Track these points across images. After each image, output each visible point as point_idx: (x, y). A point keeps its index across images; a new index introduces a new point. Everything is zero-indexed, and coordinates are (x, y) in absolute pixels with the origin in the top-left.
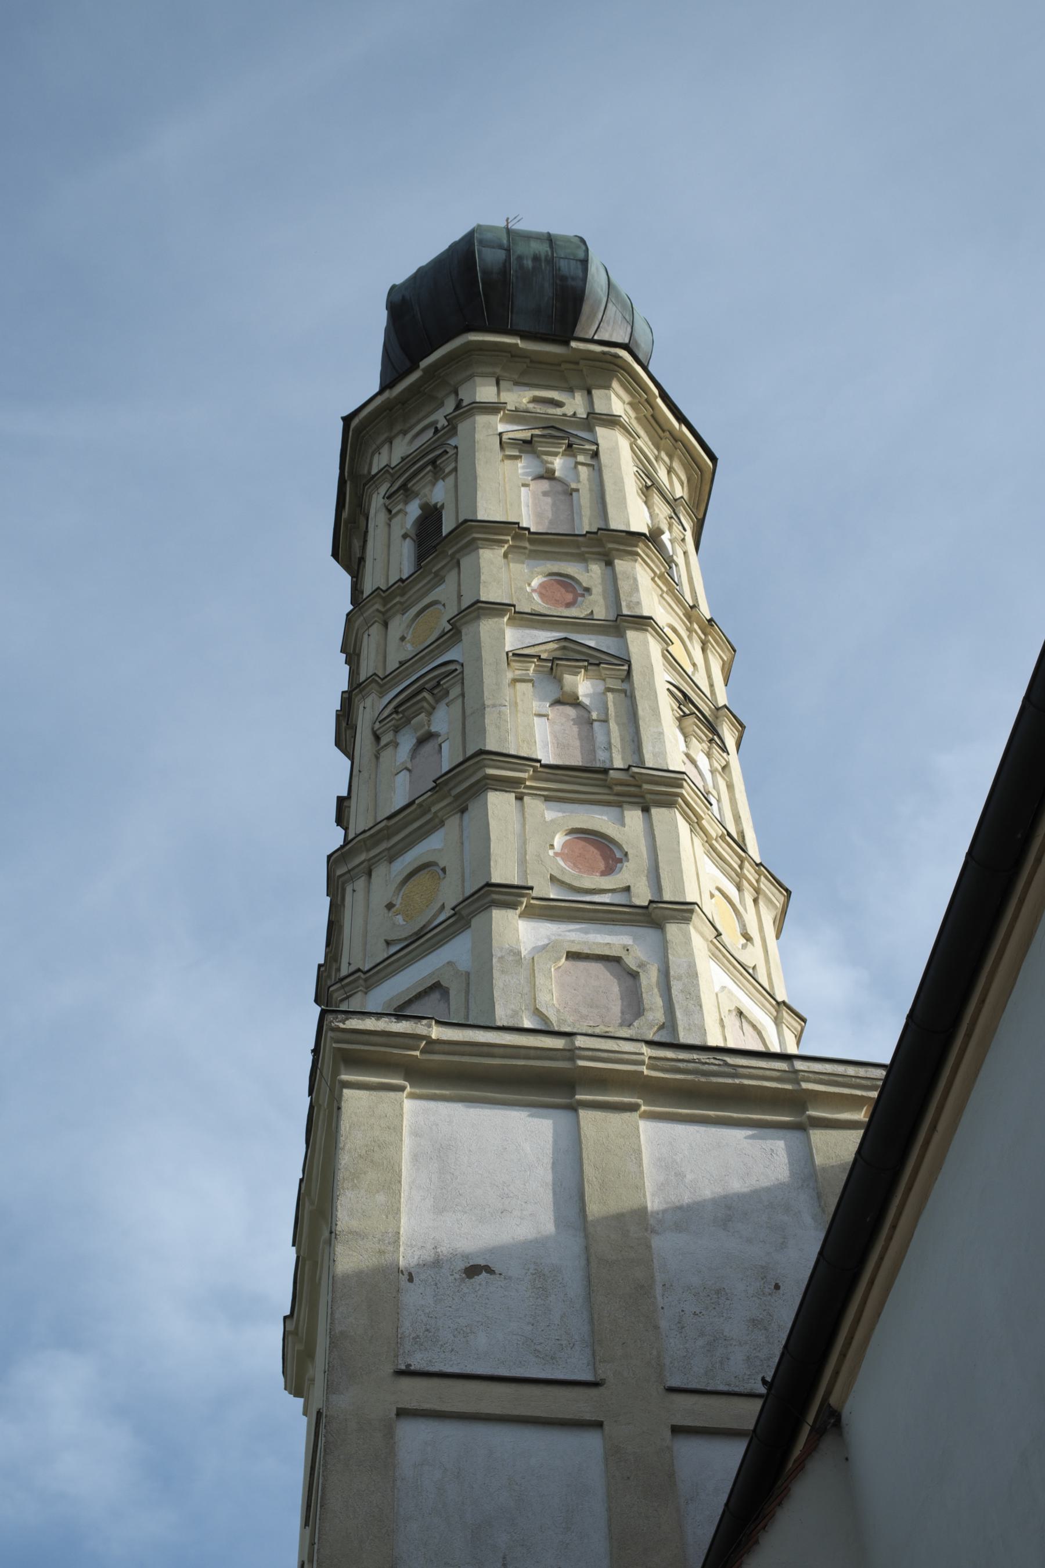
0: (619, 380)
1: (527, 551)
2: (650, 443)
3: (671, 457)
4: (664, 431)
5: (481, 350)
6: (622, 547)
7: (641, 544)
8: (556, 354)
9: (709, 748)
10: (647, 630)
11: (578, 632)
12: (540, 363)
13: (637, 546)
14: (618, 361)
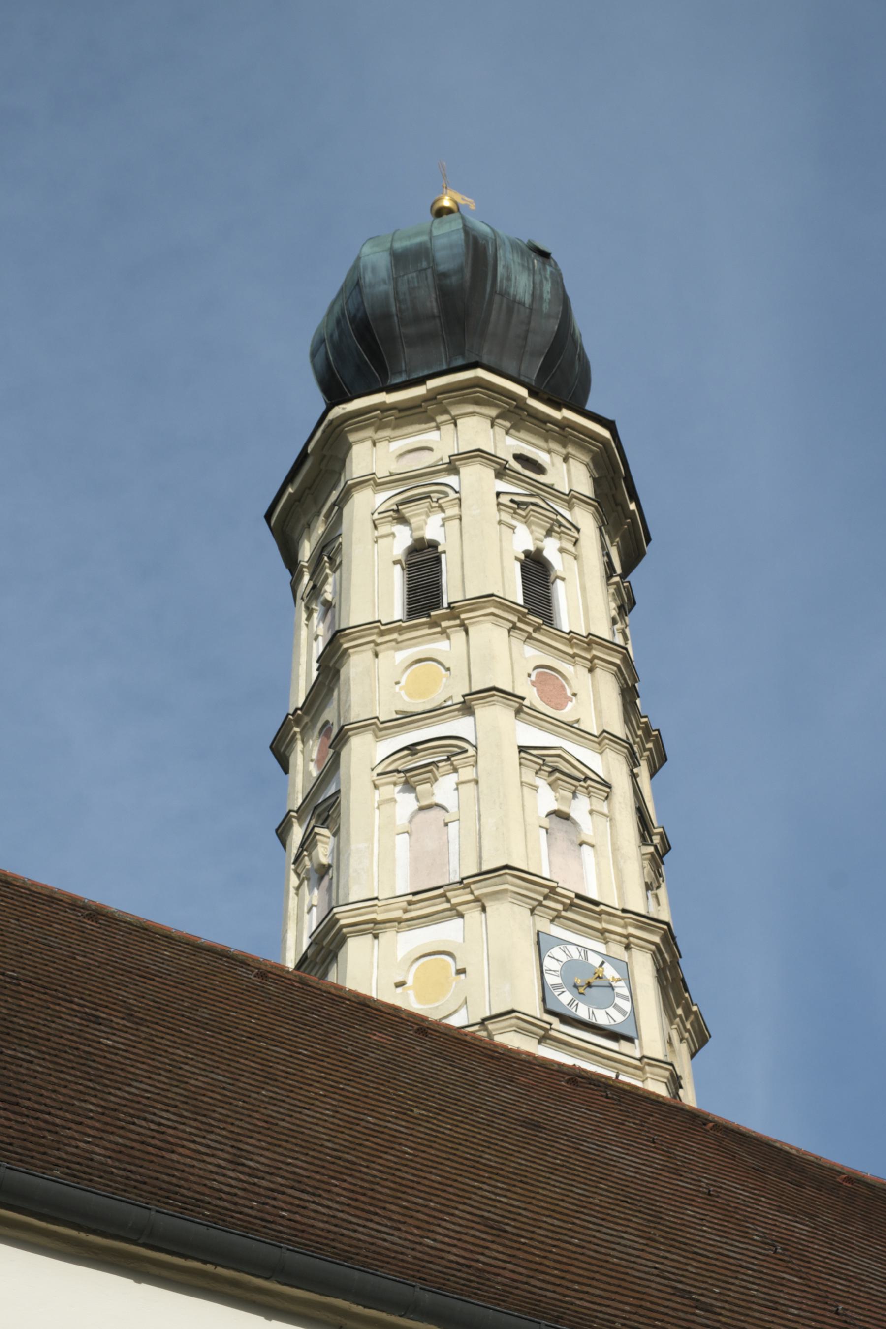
0: (351, 431)
1: (309, 724)
2: (424, 426)
3: (446, 412)
4: (420, 406)
5: (284, 521)
6: (336, 657)
7: (342, 641)
8: (311, 468)
9: (452, 764)
10: (349, 737)
11: (324, 790)
12: (314, 481)
13: (341, 645)
14: (335, 423)
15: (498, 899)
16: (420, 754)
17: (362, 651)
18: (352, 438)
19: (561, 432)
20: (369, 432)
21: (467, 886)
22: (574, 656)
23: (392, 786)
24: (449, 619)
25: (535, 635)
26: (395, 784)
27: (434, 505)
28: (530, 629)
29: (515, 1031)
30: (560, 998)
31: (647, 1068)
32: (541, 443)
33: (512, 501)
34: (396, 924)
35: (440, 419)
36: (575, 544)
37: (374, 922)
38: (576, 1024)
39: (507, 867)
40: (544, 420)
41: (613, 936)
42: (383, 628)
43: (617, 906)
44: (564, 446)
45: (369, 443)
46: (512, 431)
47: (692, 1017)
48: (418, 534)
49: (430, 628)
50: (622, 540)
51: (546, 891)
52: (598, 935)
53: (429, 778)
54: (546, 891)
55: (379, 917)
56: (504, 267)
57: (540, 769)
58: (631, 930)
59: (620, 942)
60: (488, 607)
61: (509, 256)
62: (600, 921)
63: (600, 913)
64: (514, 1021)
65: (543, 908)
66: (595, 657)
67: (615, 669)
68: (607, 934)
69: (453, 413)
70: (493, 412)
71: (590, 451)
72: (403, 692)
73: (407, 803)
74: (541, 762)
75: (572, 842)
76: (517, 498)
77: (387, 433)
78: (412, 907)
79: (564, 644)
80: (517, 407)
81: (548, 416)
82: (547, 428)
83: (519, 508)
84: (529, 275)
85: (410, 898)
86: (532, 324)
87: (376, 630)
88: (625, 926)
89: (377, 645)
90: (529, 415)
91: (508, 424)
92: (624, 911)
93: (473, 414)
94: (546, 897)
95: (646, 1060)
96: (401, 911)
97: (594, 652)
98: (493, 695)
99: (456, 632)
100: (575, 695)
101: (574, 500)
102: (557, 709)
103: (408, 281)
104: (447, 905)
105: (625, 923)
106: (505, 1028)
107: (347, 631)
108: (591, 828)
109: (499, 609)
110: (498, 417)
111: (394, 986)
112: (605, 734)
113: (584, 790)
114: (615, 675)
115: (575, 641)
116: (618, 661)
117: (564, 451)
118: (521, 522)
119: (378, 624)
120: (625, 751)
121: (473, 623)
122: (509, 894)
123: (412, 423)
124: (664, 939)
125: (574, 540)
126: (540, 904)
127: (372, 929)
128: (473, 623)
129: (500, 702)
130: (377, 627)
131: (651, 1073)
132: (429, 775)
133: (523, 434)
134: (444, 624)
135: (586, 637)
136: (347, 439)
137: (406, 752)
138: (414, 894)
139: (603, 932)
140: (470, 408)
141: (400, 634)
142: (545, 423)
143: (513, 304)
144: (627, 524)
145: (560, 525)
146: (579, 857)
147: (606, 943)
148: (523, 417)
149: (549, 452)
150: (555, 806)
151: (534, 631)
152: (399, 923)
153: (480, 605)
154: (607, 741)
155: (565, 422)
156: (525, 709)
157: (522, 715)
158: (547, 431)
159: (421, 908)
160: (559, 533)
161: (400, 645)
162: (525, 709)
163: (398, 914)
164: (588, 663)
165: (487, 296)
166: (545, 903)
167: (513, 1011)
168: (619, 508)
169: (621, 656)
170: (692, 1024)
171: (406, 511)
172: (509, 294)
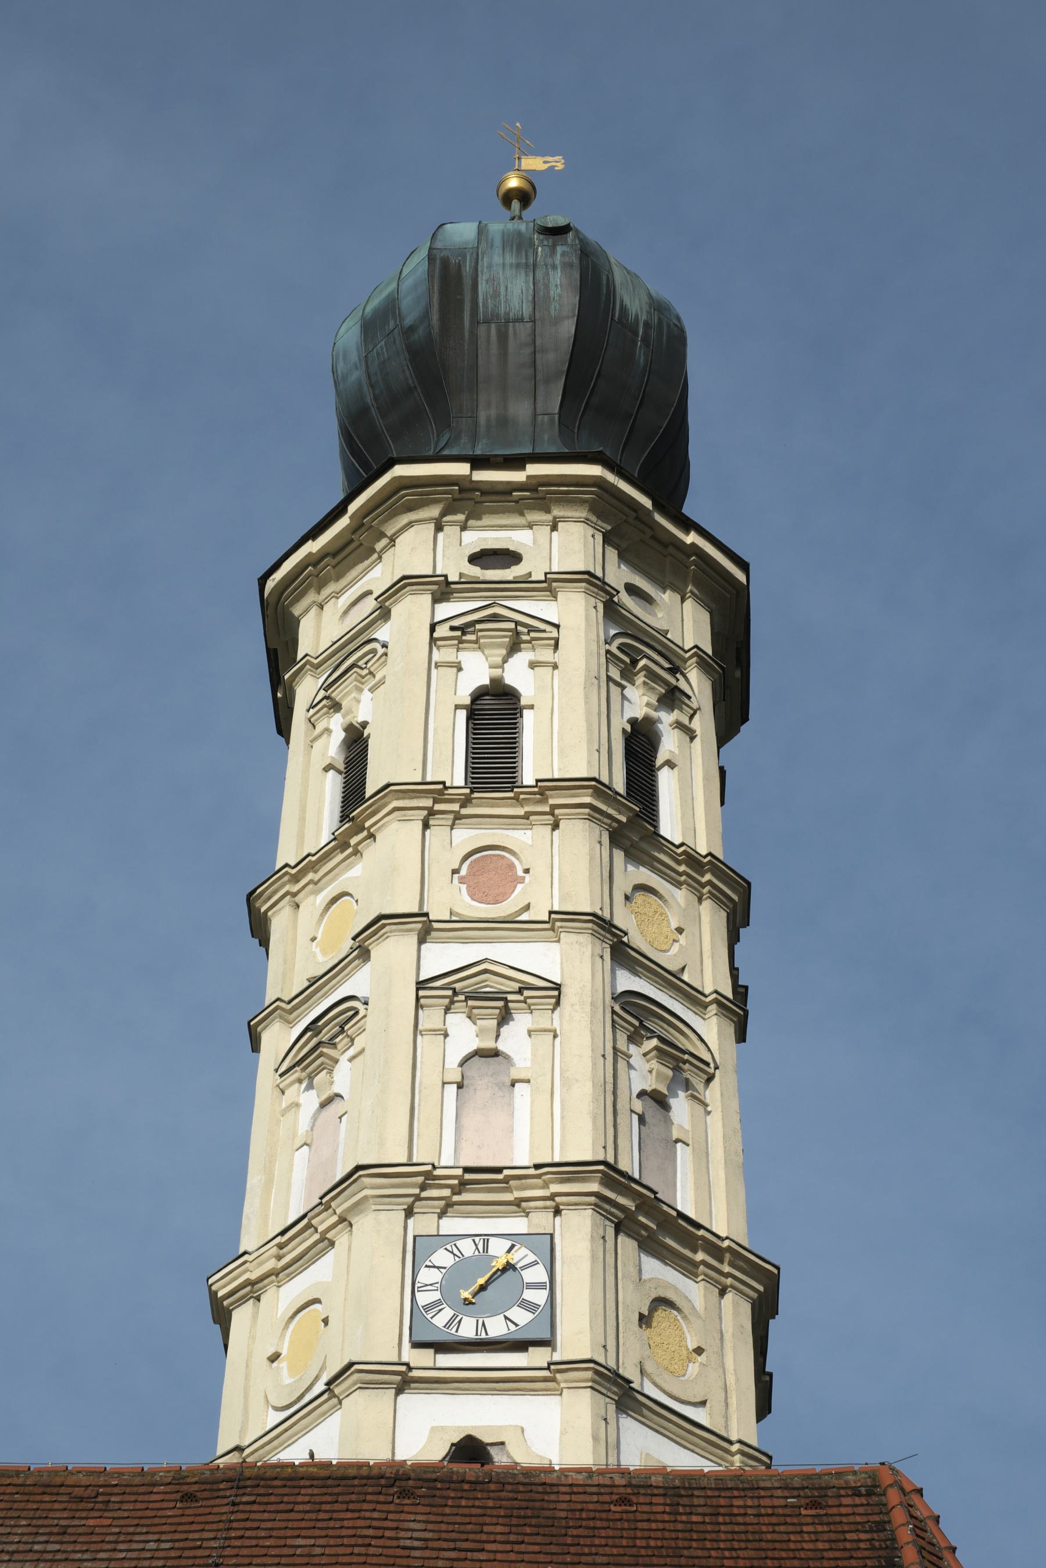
2: (367, 563)
4: (352, 541)
9: (348, 1036)
15: (362, 1212)
16: (324, 1031)
17: (280, 910)
18: (297, 610)
19: (535, 495)
20: (311, 597)
21: (328, 1207)
22: (527, 816)
23: (297, 1085)
24: (357, 834)
25: (464, 811)
26: (300, 1081)
27: (365, 672)
28: (455, 807)
29: (360, 1388)
30: (434, 1321)
31: (558, 1376)
32: (517, 520)
33: (452, 628)
34: (273, 1277)
35: (379, 546)
36: (556, 646)
37: (249, 1283)
38: (463, 1347)
39: (359, 1168)
40: (505, 491)
41: (532, 1204)
42: (294, 871)
43: (527, 1164)
44: (548, 511)
45: (314, 610)
46: (471, 523)
47: (727, 1256)
48: (349, 719)
49: (342, 852)
50: (696, 585)
51: (420, 1179)
52: (514, 1208)
53: (322, 1064)
54: (420, 1179)
55: (253, 1276)
56: (487, 281)
57: (452, 1002)
58: (555, 1188)
59: (545, 1208)
60: (390, 802)
61: (497, 259)
62: (509, 1190)
63: (507, 1180)
64: (356, 1376)
65: (424, 1202)
66: (554, 807)
67: (587, 811)
68: (524, 1204)
69: (389, 532)
70: (435, 511)
71: (583, 501)
72: (318, 951)
73: (310, 1100)
74: (449, 993)
75: (500, 1086)
76: (456, 623)
77: (331, 588)
78: (285, 1250)
79: (511, 806)
80: (461, 491)
81: (508, 483)
82: (514, 499)
83: (464, 633)
84: (527, 275)
85: (278, 1240)
86: (538, 342)
87: (286, 878)
88: (546, 1186)
89: (294, 895)
90: (484, 493)
91: (461, 517)
92: (537, 1167)
93: (410, 525)
94: (423, 1187)
95: (552, 1367)
96: (273, 1260)
97: (551, 801)
98: (384, 926)
99: (368, 846)
100: (527, 871)
101: (554, 584)
102: (496, 902)
103: (378, 354)
104: (316, 1237)
105: (544, 1181)
106: (349, 1388)
107: (258, 891)
108: (529, 1055)
109: (403, 798)
110: (443, 514)
111: (268, 1363)
112: (553, 916)
113: (523, 1005)
114: (590, 819)
115: (522, 796)
116: (587, 800)
117: (549, 517)
118: (474, 649)
119: (287, 869)
120: (590, 925)
121: (379, 828)
122: (371, 1201)
123: (355, 565)
124: (607, 1181)
125: (553, 642)
126: (418, 1198)
127: (251, 1292)
128: (379, 828)
129: (395, 931)
130: (287, 873)
131: (566, 1381)
132: (321, 1059)
133: (487, 520)
134: (353, 841)
135: (536, 786)
136: (293, 615)
137: (309, 1034)
138: (283, 1233)
139: (518, 1203)
140: (404, 519)
141: (316, 872)
142: (509, 493)
143: (505, 324)
144: (694, 563)
145: (531, 629)
146: (510, 1104)
147: (527, 1215)
148: (479, 499)
149: (530, 526)
150: (474, 1044)
151: (462, 806)
152: (277, 1275)
153: (379, 803)
154: (558, 924)
155: (534, 481)
156: (436, 925)
157: (434, 934)
158: (517, 502)
159: (293, 1249)
160: (529, 642)
161: (319, 884)
162: (436, 925)
163: (271, 1264)
164: (550, 817)
165: (467, 334)
166: (424, 1194)
167: (351, 1364)
168: (671, 549)
169: (590, 791)
170: (731, 1264)
171: (337, 694)
172: (498, 316)
